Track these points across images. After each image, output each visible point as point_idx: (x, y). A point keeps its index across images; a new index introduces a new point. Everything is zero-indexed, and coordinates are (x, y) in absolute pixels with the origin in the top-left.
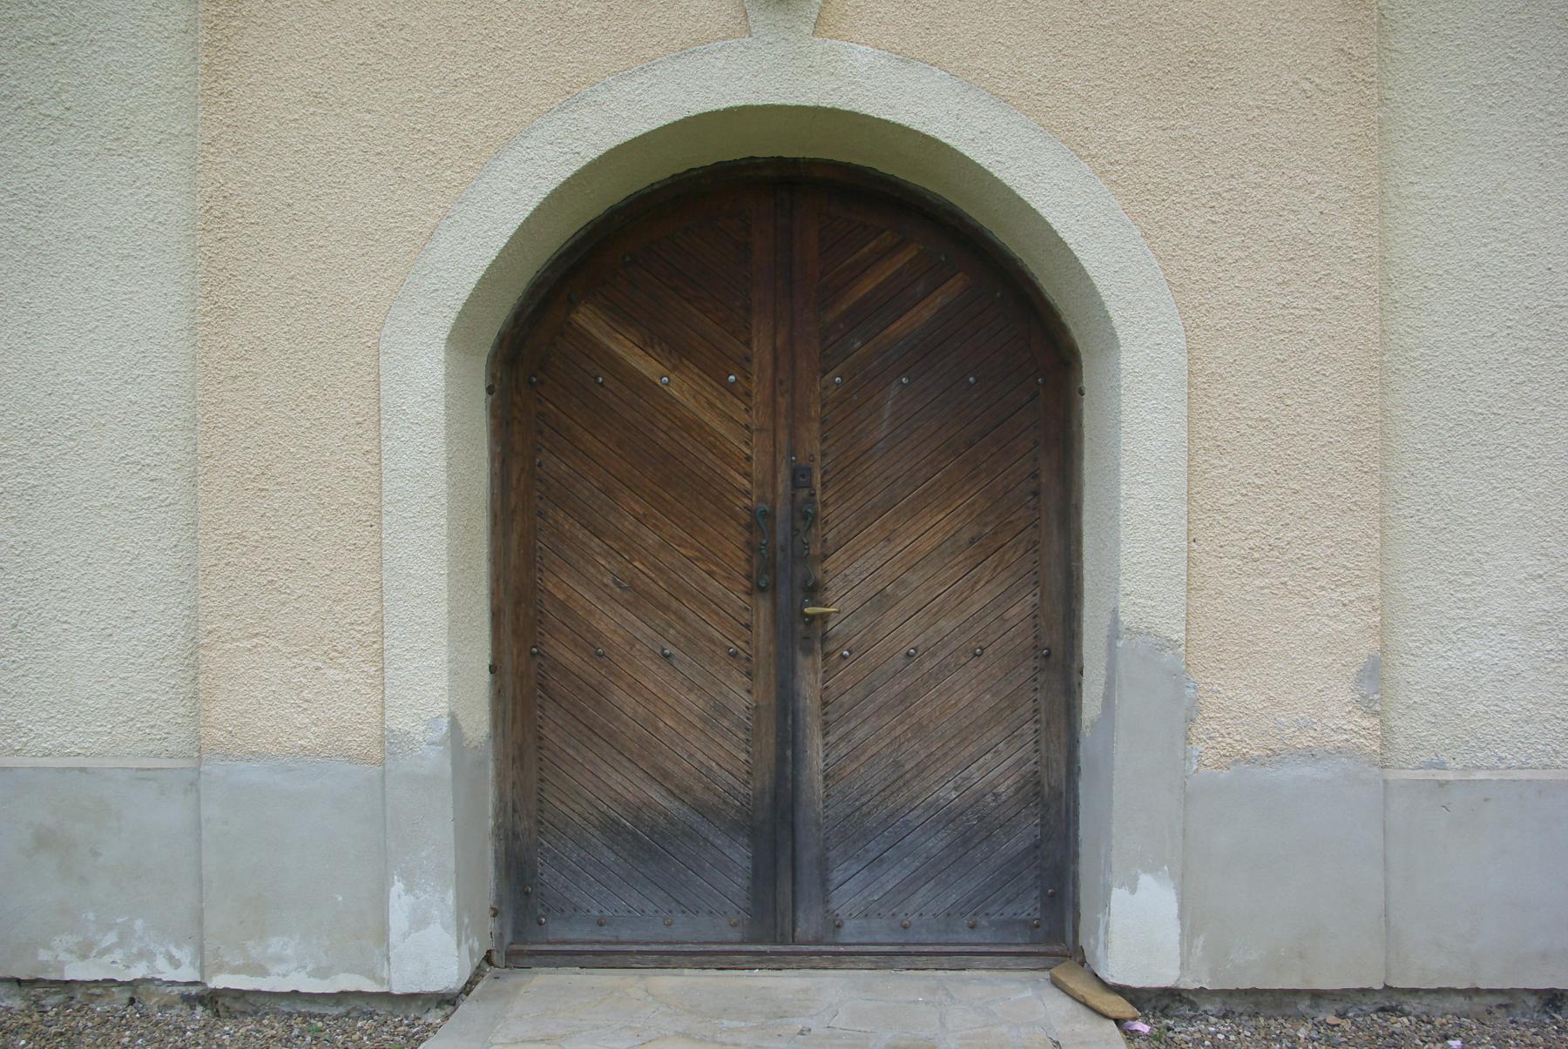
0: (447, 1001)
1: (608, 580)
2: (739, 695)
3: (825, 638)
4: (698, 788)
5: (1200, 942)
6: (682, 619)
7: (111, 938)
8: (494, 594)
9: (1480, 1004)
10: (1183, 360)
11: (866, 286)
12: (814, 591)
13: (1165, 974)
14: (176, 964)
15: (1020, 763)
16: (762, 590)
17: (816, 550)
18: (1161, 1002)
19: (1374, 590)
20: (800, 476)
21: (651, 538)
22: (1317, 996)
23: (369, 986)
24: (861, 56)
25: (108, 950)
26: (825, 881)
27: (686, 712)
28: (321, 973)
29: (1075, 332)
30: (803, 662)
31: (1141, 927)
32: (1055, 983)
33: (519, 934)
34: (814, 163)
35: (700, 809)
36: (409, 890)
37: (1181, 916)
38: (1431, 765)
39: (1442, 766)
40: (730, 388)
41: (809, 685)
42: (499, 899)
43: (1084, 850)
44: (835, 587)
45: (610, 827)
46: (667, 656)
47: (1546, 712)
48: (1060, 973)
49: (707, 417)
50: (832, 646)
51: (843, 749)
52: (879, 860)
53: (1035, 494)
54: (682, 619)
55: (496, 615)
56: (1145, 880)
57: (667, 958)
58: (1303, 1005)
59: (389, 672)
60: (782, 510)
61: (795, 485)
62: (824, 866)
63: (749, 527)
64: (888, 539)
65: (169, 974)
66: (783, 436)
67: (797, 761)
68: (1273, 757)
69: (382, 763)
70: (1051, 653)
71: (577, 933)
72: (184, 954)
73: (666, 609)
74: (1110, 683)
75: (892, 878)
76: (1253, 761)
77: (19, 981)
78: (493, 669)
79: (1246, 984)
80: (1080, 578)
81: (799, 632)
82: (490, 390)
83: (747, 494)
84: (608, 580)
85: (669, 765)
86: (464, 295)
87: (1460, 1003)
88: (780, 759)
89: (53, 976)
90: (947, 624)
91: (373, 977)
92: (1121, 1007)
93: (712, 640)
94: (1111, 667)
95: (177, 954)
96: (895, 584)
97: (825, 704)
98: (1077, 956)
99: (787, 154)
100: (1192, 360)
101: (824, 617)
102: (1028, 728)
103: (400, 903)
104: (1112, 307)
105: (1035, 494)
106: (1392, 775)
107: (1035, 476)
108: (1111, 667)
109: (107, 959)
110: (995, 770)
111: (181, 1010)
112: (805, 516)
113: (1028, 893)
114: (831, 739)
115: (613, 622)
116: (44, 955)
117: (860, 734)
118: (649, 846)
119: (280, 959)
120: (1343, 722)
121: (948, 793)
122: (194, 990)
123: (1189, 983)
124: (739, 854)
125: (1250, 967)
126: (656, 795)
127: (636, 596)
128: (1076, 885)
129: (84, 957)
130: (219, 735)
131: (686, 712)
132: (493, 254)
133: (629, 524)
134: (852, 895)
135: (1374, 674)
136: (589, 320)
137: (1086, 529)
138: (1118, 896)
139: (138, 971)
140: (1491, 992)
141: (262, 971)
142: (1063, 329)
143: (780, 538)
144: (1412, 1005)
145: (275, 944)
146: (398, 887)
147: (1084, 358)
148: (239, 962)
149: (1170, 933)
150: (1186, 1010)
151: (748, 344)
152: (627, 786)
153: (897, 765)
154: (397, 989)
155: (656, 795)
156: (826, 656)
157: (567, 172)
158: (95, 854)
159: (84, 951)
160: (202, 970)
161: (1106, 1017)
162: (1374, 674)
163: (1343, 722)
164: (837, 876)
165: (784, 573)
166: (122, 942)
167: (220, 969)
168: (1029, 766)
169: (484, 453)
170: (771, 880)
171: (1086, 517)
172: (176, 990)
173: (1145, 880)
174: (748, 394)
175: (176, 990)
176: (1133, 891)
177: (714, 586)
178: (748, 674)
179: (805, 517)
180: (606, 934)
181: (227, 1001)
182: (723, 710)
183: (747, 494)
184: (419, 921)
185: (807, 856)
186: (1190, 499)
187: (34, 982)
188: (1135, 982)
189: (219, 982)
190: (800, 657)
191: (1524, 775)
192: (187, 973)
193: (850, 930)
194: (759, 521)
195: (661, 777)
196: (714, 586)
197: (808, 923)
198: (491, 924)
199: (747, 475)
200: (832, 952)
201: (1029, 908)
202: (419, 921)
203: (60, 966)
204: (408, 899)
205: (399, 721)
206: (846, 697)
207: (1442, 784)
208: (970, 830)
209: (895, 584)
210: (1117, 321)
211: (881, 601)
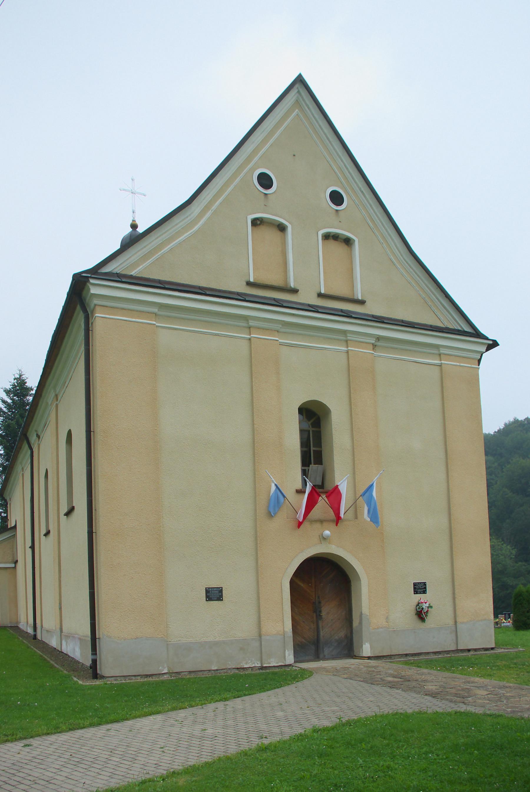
12: (320, 612)
24: (333, 546)
26: (323, 650)
28: (277, 663)
29: (350, 577)
31: (367, 650)
72: (259, 663)
75: (331, 649)
77: (238, 668)
81: (319, 617)
90: (335, 616)
103: (287, 653)
113: (348, 648)
121: (337, 638)
126: (303, 640)
135: (387, 618)
138: (364, 646)
139: (253, 665)
141: (270, 663)
142: (349, 578)
145: (272, 660)
146: (286, 651)
159: (246, 664)
160: (262, 664)
162: (387, 618)
166: (251, 662)
167: (265, 664)
179: (320, 603)
181: (96, 720)
184: (289, 655)
189: (265, 665)
192: (259, 665)
197: (321, 656)
202: (289, 655)
209: (330, 611)
211: (328, 613)
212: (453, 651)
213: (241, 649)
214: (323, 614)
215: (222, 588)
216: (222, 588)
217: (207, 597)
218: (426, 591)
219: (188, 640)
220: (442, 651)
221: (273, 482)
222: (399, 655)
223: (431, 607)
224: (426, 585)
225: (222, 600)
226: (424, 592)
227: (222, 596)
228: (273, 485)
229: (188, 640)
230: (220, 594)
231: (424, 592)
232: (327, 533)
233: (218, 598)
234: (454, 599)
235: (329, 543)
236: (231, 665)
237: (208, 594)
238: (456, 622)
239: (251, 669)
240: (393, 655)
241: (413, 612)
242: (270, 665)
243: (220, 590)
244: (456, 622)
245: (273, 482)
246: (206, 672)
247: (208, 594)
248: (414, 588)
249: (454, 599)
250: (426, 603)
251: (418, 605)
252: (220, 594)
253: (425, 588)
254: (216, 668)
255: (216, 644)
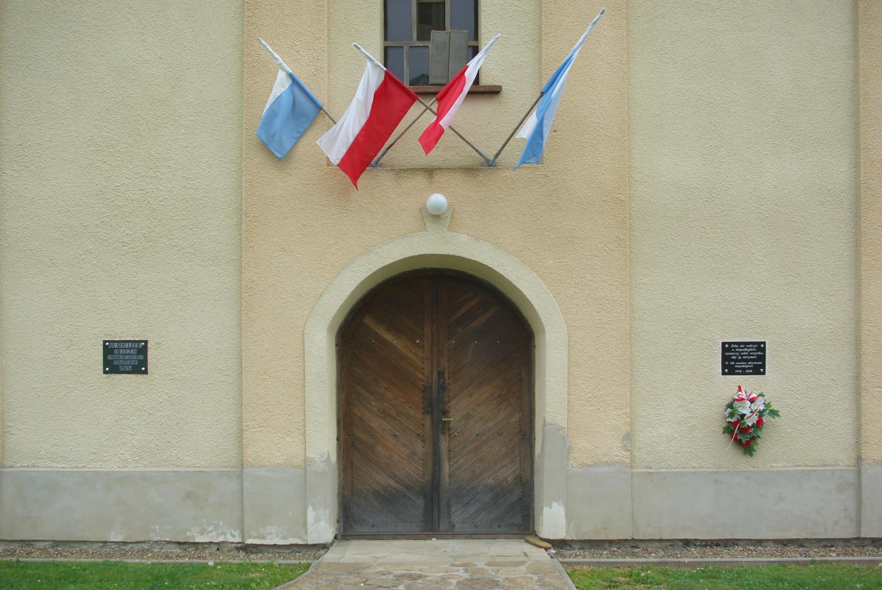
0: (325, 547)
1: (375, 409)
2: (420, 448)
3: (449, 429)
4: (406, 480)
5: (572, 524)
6: (400, 422)
7: (212, 528)
8: (338, 414)
9: (663, 545)
10: (566, 337)
11: (464, 310)
12: (445, 413)
13: (561, 535)
14: (233, 536)
15: (515, 471)
16: (428, 413)
17: (446, 399)
18: (560, 544)
19: (628, 410)
20: (441, 375)
21: (390, 396)
22: (611, 542)
23: (300, 542)
24: (463, 238)
25: (211, 532)
26: (449, 511)
27: (402, 454)
29: (533, 327)
30: (442, 437)
31: (553, 520)
32: (527, 541)
33: (345, 529)
34: (446, 270)
35: (408, 488)
36: (314, 510)
37: (566, 516)
38: (647, 467)
39: (651, 468)
40: (417, 344)
41: (444, 445)
42: (339, 516)
43: (536, 499)
44: (452, 412)
45: (376, 494)
46: (396, 436)
47: (684, 450)
48: (528, 538)
49: (411, 356)
50: (452, 432)
51: (455, 466)
52: (468, 503)
53: (520, 380)
54: (400, 422)
55: (338, 421)
56: (554, 504)
57: (396, 536)
58: (607, 545)
59: (308, 438)
60: (435, 386)
61: (439, 378)
62: (449, 506)
63: (423, 392)
64: (470, 396)
65: (231, 540)
66: (435, 361)
67: (440, 471)
68: (596, 464)
69: (305, 468)
70: (525, 434)
71: (365, 530)
72: (237, 533)
73: (395, 419)
74: (543, 441)
75: (472, 509)
76: (589, 466)
77: (179, 543)
78: (338, 439)
79: (587, 538)
80: (534, 408)
81: (440, 427)
82: (336, 345)
83: (423, 380)
84: (375, 409)
85: (396, 472)
86: (333, 315)
87: (657, 544)
88: (434, 470)
89: (192, 541)
90: (490, 424)
91: (301, 538)
92: (548, 545)
93: (411, 430)
94: (544, 436)
95: (234, 533)
96: (472, 411)
97: (449, 451)
98: (534, 534)
99: (438, 267)
100: (569, 337)
101: (449, 422)
102: (518, 459)
103: (311, 514)
104: (543, 319)
105: (520, 380)
106: (634, 470)
107: (520, 374)
108: (544, 436)
109: (210, 535)
110: (507, 473)
111: (235, 553)
112: (443, 388)
113: (515, 513)
114: (452, 463)
115: (377, 424)
116: (188, 534)
117: (461, 461)
118: (389, 500)
119: (270, 534)
120: (618, 453)
122: (239, 545)
123: (569, 538)
124: (420, 502)
125: (589, 533)
126: (392, 483)
127: (385, 415)
128: (533, 510)
129: (202, 534)
130: (250, 460)
131: (402, 454)
132: (342, 302)
133: (382, 391)
134: (459, 515)
135: (628, 437)
136: (368, 321)
137: (536, 392)
138: (546, 510)
139: (221, 539)
140: (667, 540)
141: (264, 538)
142: (529, 325)
143: (434, 395)
144: (642, 545)
145: (268, 529)
146: (310, 509)
147: (536, 336)
148: (256, 535)
149: (562, 522)
150: (568, 548)
151: (423, 330)
152: (381, 479)
153: (474, 471)
154: (310, 543)
155: (392, 483)
156: (450, 435)
157: (366, 275)
158: (206, 500)
160: (243, 538)
161: (542, 547)
162: (628, 437)
163: (618, 453)
164: (453, 509)
165: (435, 407)
166: (216, 528)
167: (250, 537)
168: (518, 472)
169: (335, 367)
170: (429, 510)
171: (536, 388)
172: (233, 545)
173: (554, 504)
174: (423, 347)
175: (233, 545)
176: (550, 507)
177: (412, 412)
178: (424, 441)
179: (443, 388)
180: (375, 530)
182: (415, 453)
183: (423, 380)
184: (317, 520)
185: (443, 503)
186: (569, 381)
187: (184, 543)
188: (551, 538)
189: (249, 541)
190: (441, 436)
191: (677, 470)
192: (238, 539)
193: (458, 528)
194: (427, 389)
195: (393, 476)
196: (412, 412)
197: (444, 525)
198: (336, 525)
199: (423, 374)
200: (451, 534)
201: (518, 520)
202: (317, 520)
203: (194, 538)
204: (314, 513)
205: (310, 455)
206: (456, 449)
207: (650, 473)
208: (498, 493)
209: (472, 411)
210: (545, 325)
211: (468, 417)
212: (846, 541)
213: (188, 496)
214: (453, 418)
215: (146, 342)
216: (146, 342)
217: (106, 363)
218: (763, 366)
219: (55, 465)
220: (807, 540)
221: (284, 70)
222: (661, 541)
223: (774, 413)
224: (764, 350)
225: (146, 372)
226: (758, 369)
227: (144, 362)
228: (281, 75)
229: (55, 465)
230: (141, 357)
231: (758, 369)
232: (438, 199)
233: (133, 366)
234: (858, 392)
235: (450, 228)
236: (161, 533)
237: (109, 357)
238: (859, 459)
239: (215, 547)
240: (642, 541)
241: (718, 427)
242: (265, 542)
243: (142, 348)
244: (859, 459)
245: (284, 70)
246: (96, 546)
247: (109, 357)
248: (725, 358)
249: (858, 392)
250: (752, 401)
251: (730, 406)
252: (141, 357)
253: (762, 358)
254: (120, 539)
255: (124, 479)
